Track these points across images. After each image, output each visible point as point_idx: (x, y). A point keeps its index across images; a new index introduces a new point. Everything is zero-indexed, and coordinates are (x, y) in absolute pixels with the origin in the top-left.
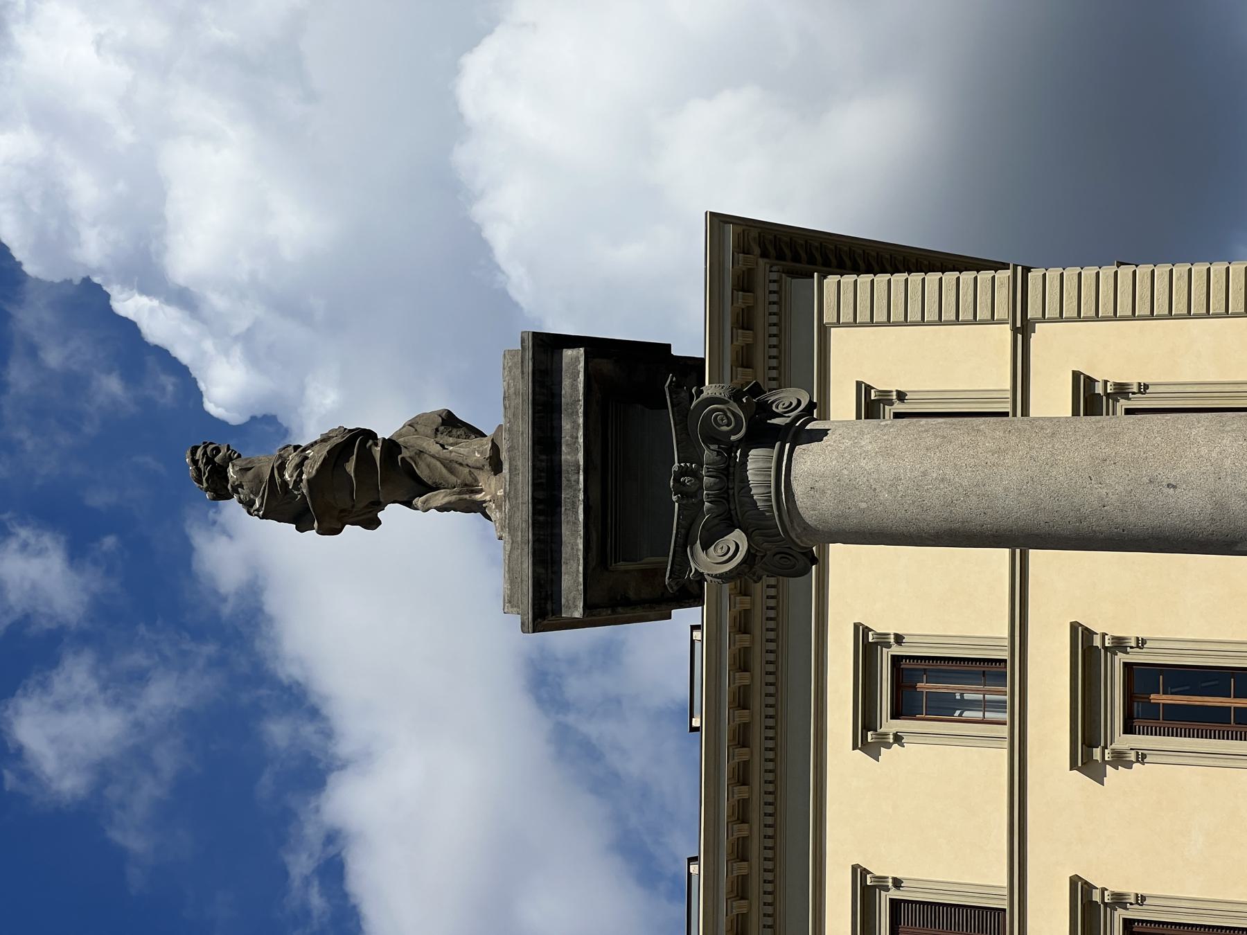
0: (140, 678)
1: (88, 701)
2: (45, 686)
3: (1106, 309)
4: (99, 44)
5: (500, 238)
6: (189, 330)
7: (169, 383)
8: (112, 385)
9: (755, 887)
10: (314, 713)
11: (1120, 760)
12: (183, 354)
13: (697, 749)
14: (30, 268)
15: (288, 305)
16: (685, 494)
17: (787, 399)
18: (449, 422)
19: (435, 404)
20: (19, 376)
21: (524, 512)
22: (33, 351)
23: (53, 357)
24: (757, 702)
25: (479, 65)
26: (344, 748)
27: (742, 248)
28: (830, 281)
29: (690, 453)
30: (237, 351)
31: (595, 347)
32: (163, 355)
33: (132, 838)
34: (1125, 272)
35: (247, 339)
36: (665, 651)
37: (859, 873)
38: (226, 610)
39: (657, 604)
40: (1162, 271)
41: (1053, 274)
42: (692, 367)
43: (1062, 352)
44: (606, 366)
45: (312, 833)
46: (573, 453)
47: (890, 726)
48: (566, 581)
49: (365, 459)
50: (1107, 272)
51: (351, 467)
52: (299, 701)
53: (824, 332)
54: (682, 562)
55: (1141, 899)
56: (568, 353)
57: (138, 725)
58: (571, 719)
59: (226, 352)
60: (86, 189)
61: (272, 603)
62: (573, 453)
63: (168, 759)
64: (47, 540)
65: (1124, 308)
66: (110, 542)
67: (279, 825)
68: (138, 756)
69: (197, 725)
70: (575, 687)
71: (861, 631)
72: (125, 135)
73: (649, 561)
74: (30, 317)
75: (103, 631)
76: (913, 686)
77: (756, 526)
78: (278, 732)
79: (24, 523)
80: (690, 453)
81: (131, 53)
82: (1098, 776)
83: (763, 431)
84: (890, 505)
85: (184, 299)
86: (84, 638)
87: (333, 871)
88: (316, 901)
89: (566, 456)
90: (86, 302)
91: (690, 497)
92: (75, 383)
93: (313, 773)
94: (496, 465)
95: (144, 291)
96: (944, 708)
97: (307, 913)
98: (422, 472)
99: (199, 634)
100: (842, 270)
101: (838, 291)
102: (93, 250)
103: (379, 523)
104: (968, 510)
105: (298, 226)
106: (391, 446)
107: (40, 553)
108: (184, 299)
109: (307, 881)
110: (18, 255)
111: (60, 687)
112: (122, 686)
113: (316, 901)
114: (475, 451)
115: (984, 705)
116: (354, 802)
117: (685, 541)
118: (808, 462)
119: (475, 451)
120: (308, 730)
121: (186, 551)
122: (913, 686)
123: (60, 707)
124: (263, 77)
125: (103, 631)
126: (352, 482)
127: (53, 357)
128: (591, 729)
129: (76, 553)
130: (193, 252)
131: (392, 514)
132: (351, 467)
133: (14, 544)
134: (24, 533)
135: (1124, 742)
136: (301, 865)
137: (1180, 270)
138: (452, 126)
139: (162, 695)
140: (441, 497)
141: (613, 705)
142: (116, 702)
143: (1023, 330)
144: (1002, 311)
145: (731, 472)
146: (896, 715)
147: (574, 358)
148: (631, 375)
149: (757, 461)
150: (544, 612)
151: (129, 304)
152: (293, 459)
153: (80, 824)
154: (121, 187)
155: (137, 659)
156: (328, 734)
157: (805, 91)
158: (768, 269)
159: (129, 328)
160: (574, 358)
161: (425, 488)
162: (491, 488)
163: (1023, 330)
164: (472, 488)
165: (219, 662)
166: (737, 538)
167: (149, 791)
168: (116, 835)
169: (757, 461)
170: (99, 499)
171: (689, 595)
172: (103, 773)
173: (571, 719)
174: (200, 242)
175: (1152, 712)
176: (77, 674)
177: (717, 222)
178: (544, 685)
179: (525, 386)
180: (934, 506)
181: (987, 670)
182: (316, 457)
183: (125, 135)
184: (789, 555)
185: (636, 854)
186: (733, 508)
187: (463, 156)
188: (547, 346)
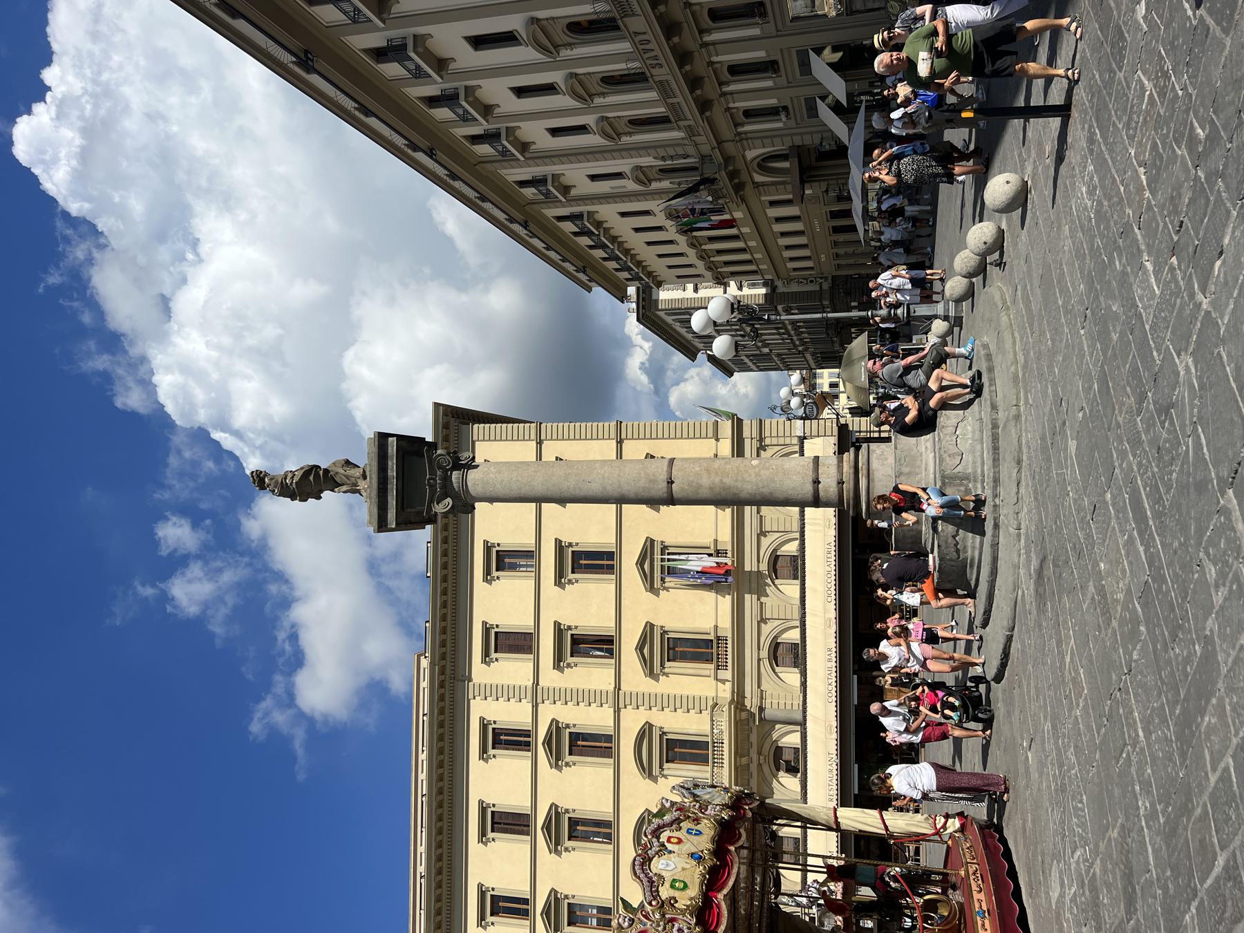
0: (220, 571)
1: (200, 579)
2: (183, 574)
3: (566, 436)
4: (207, 344)
5: (358, 415)
6: (241, 444)
7: (232, 464)
8: (210, 465)
9: (449, 630)
10: (287, 582)
11: (570, 582)
12: (237, 453)
13: (429, 589)
14: (178, 423)
15: (278, 438)
16: (430, 486)
17: (465, 456)
18: (348, 463)
19: (342, 457)
20: (173, 461)
21: (375, 493)
22: (179, 452)
23: (187, 455)
24: (450, 567)
25: (350, 355)
26: (297, 593)
27: (445, 414)
28: (476, 426)
29: (433, 473)
30: (258, 453)
31: (400, 438)
32: (232, 455)
33: (217, 628)
34: (572, 425)
35: (261, 448)
36: (419, 543)
37: (485, 623)
38: (254, 545)
39: (420, 524)
40: (583, 425)
41: (549, 425)
42: (433, 446)
43: (551, 450)
44: (404, 443)
45: (286, 624)
46: (392, 472)
47: (495, 574)
48: (389, 516)
49: (317, 475)
50: (566, 425)
51: (311, 478)
52: (281, 577)
53: (473, 443)
54: (430, 509)
55: (576, 627)
56: (390, 439)
57: (220, 588)
58: (383, 580)
59: (253, 453)
60: (200, 395)
61: (271, 542)
62: (392, 472)
63: (230, 600)
64: (183, 521)
65: (572, 437)
66: (208, 522)
67: (274, 622)
68: (219, 599)
69: (240, 587)
70: (385, 569)
71: (486, 542)
72: (215, 376)
73: (419, 508)
74: (177, 440)
75: (205, 554)
76: (504, 560)
77: (455, 496)
78: (273, 588)
79: (174, 514)
80: (433, 473)
81: (219, 348)
82: (486, 760)
83: (457, 466)
84: (500, 490)
85: (238, 434)
86: (198, 557)
87: (294, 637)
88: (288, 647)
89: (390, 473)
90: (201, 435)
91: (432, 487)
92: (195, 464)
93: (286, 603)
94: (364, 477)
95: (223, 431)
96: (513, 567)
97: (284, 652)
98: (338, 479)
99: (242, 554)
100: (479, 422)
101: (478, 429)
102: (202, 417)
103: (319, 498)
104: (526, 490)
105: (280, 408)
106: (326, 471)
107: (181, 526)
108: (238, 434)
109: (284, 641)
110: (174, 418)
111: (189, 575)
112: (213, 574)
113: (288, 647)
114: (357, 473)
115: (527, 566)
116: (300, 612)
117: (431, 501)
118: (472, 475)
119: (357, 473)
120: (284, 587)
121: (238, 525)
122: (504, 560)
123: (190, 582)
124: (268, 358)
125: (205, 554)
126: (310, 484)
127: (187, 455)
128: (392, 583)
129: (195, 525)
130: (241, 419)
131: (326, 494)
132: (311, 478)
133: (170, 523)
134: (174, 519)
135: (571, 576)
136: (282, 636)
137: (589, 424)
138: (341, 376)
139: (228, 577)
140: (344, 488)
141: (397, 574)
142: (210, 579)
143: (540, 443)
144: (533, 437)
145: (447, 479)
146: (497, 570)
147: (392, 440)
148: (410, 446)
149: (455, 475)
150: (382, 526)
151: (216, 435)
152: (290, 475)
153: (198, 623)
154: (213, 395)
155: (219, 564)
156: (292, 589)
157: (465, 366)
158: (455, 421)
159: (217, 444)
160: (392, 440)
161: (339, 485)
162: (363, 485)
163: (540, 443)
164: (356, 485)
165: (250, 565)
166: (449, 500)
167: (223, 611)
168: (211, 627)
169: (455, 475)
170: (204, 506)
171: (432, 520)
172: (206, 605)
173: (383, 580)
174: (244, 413)
175: (580, 566)
176: (196, 569)
177: (437, 405)
178: (373, 567)
179: (375, 450)
180: (514, 494)
181: (528, 554)
182: (299, 475)
183: (215, 376)
184: (465, 505)
185: (405, 626)
186: (448, 490)
187: (344, 386)
188: (383, 437)
